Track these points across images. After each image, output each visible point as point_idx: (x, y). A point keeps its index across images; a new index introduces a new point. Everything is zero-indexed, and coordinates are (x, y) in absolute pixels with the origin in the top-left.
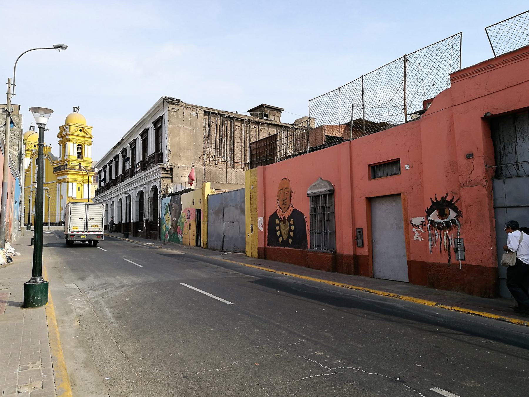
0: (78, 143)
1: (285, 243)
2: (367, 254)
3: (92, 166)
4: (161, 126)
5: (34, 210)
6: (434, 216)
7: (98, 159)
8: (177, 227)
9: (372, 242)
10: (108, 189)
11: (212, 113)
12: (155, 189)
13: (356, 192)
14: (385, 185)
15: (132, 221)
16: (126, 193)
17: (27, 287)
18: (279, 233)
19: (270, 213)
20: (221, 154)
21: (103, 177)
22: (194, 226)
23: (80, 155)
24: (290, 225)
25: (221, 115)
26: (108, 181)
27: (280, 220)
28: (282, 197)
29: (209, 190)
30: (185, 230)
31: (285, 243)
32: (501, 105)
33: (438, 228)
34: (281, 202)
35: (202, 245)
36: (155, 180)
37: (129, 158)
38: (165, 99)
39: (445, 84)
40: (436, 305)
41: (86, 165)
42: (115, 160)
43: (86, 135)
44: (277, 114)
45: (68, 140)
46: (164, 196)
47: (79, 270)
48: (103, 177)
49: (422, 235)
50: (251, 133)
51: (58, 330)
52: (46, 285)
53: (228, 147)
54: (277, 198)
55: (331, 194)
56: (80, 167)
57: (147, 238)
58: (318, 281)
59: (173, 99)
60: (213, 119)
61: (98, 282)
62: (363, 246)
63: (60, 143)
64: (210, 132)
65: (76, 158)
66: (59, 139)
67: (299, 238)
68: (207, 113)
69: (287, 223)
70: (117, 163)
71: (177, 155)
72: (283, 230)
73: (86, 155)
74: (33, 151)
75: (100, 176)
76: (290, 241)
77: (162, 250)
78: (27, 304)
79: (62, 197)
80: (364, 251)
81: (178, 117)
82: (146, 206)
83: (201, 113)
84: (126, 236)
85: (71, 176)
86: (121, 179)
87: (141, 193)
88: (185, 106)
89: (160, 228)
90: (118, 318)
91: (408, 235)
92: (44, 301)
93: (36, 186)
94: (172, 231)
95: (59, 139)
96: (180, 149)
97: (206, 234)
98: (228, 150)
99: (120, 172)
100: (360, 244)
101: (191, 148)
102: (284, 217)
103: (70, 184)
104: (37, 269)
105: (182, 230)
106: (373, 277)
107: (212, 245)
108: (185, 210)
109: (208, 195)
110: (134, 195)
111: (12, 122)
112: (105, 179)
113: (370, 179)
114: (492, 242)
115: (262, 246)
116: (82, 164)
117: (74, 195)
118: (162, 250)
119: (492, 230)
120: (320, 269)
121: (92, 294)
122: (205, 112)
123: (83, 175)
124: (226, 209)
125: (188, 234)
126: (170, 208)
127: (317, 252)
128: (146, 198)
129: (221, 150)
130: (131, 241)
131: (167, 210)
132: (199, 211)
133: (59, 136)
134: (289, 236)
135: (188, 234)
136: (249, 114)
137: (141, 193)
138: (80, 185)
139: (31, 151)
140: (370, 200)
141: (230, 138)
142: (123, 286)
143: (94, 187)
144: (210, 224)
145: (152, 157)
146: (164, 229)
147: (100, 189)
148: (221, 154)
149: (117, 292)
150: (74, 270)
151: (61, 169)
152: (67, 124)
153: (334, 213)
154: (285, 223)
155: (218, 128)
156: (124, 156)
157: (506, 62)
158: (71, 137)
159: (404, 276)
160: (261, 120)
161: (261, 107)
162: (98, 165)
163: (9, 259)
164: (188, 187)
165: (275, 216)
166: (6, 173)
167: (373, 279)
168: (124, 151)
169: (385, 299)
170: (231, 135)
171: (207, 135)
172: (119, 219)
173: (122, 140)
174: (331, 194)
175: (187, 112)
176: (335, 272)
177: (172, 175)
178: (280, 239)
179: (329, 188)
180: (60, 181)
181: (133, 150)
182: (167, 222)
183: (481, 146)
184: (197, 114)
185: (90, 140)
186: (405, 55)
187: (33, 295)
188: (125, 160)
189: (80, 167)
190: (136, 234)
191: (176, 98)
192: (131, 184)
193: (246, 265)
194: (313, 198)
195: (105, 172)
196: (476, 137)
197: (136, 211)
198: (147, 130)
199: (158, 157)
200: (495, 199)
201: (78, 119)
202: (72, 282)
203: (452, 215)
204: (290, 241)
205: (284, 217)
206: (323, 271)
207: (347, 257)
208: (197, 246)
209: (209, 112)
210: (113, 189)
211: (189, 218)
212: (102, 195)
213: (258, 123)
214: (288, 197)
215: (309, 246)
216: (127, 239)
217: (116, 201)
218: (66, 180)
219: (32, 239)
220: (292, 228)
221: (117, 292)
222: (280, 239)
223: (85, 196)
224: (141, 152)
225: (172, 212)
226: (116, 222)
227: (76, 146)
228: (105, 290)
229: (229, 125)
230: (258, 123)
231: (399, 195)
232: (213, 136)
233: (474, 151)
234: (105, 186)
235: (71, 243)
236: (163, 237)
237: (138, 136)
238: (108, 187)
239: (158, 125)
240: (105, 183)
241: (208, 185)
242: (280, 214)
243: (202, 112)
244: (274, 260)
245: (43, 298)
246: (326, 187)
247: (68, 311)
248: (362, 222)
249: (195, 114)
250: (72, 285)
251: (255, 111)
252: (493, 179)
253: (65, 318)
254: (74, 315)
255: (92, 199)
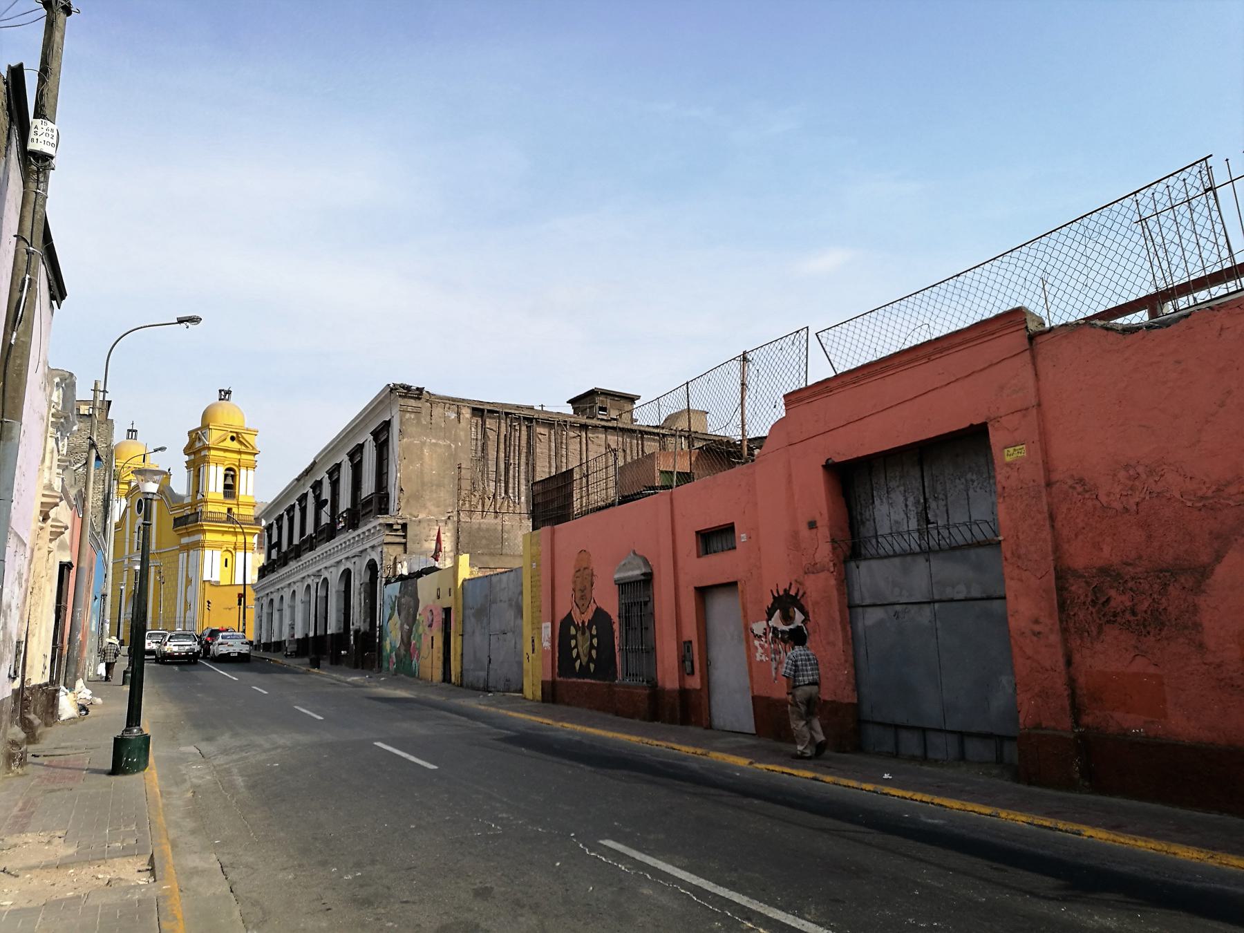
0: (228, 464)
1: (585, 671)
2: (699, 687)
3: (251, 512)
4: (387, 440)
5: (130, 610)
6: (776, 621)
7: (269, 496)
8: (409, 643)
9: (707, 664)
10: (285, 564)
11: (489, 411)
12: (372, 566)
13: (682, 577)
14: (717, 567)
15: (329, 632)
16: (318, 574)
17: (119, 743)
18: (574, 655)
19: (561, 615)
20: (506, 492)
21: (275, 540)
22: (439, 642)
23: (230, 490)
24: (592, 637)
25: (507, 414)
26: (285, 547)
27: (577, 627)
28: (579, 587)
29: (465, 572)
30: (425, 650)
31: (585, 671)
32: (848, 447)
33: (783, 640)
34: (579, 594)
35: (453, 679)
36: (373, 547)
37: (326, 501)
38: (392, 389)
39: (781, 412)
40: (751, 763)
41: (244, 511)
42: (330, 478)
43: (243, 448)
44: (627, 407)
45: (205, 460)
46: (388, 582)
47: (204, 724)
48: (275, 540)
49: (766, 652)
50: (571, 447)
51: (161, 802)
52: (147, 739)
53: (523, 476)
54: (572, 586)
55: (647, 580)
56: (230, 518)
57: (356, 667)
58: (610, 734)
59: (408, 388)
60: (490, 423)
61: (236, 742)
62: (693, 673)
63: (189, 465)
64: (484, 448)
65: (222, 497)
66: (187, 458)
67: (605, 665)
68: (480, 411)
69: (587, 634)
70: (303, 511)
71: (417, 497)
72: (582, 647)
73: (242, 491)
74: (133, 484)
75: (270, 537)
76: (592, 666)
77: (374, 690)
78: (118, 768)
79: (189, 581)
80: (694, 682)
81: (419, 422)
82: (357, 600)
83: (467, 413)
84: (315, 664)
85: (209, 537)
86: (310, 544)
87: (347, 574)
88: (434, 400)
89: (380, 647)
90: (252, 787)
91: (750, 649)
92: (142, 764)
93: (138, 567)
94: (402, 652)
95: (187, 458)
96: (423, 484)
97: (459, 658)
98: (523, 482)
99: (310, 530)
100: (689, 670)
101: (446, 481)
102: (583, 623)
103: (208, 552)
104: (134, 716)
105: (419, 649)
106: (710, 727)
107: (469, 678)
108: (425, 609)
109: (465, 580)
110: (334, 576)
111: (98, 458)
112: (279, 544)
113: (698, 556)
114: (846, 661)
115: (549, 678)
116: (235, 510)
117: (216, 578)
118: (374, 690)
119: (845, 642)
120: (632, 718)
121: (221, 760)
122: (474, 409)
123: (235, 534)
124: (494, 606)
125: (429, 661)
126: (398, 606)
127: (628, 687)
128: (356, 583)
129: (507, 483)
130: (326, 676)
131: (392, 609)
132: (447, 611)
133: (187, 451)
134: (590, 659)
135: (429, 661)
136: (569, 410)
137: (347, 574)
138: (228, 556)
139: (129, 483)
140: (703, 593)
141: (527, 460)
142: (276, 748)
143: (257, 559)
144: (466, 636)
145: (368, 502)
146: (388, 647)
147: (269, 565)
148: (506, 492)
149: (264, 757)
150: (197, 726)
151: (189, 520)
152: (205, 426)
153: (652, 614)
154: (583, 633)
155: (502, 440)
156: (317, 497)
157: (844, 385)
158: (213, 452)
159: (750, 727)
160: (589, 422)
161: (592, 393)
162: (267, 513)
163: (83, 708)
164: (432, 563)
165: (568, 620)
166: (83, 551)
167: (709, 732)
168: (317, 486)
169: (685, 759)
170: (528, 453)
171: (479, 454)
172: (304, 627)
173: (314, 464)
174: (647, 580)
175: (438, 411)
176: (652, 720)
177: (405, 537)
178: (577, 664)
179: (643, 570)
180: (187, 548)
181: (335, 484)
182: (393, 638)
183: (825, 512)
184: (459, 414)
185: (251, 457)
186: (745, 353)
187: (127, 755)
188: (320, 504)
189: (230, 518)
190: (336, 661)
191: (415, 384)
192: (328, 555)
193: (511, 713)
194: (623, 586)
195: (291, 520)
196: (816, 496)
197: (338, 611)
198: (338, 466)
199: (381, 502)
200: (850, 595)
201: (229, 417)
202: (191, 744)
203: (799, 617)
204: (592, 666)
205: (583, 623)
206: (637, 721)
207: (671, 692)
208: (444, 680)
209: (482, 410)
210: (293, 565)
211: (430, 626)
212: (273, 577)
213: (584, 427)
214: (588, 586)
215: (620, 676)
216: (316, 670)
217: (287, 594)
218: (199, 546)
219: (125, 672)
220: (595, 641)
221: (264, 757)
222: (577, 664)
223: (239, 581)
224: (347, 493)
225: (403, 615)
226: (299, 635)
227: (221, 471)
228: (244, 754)
229: (524, 433)
230: (584, 427)
231: (734, 584)
232: (490, 457)
233: (818, 518)
234: (279, 558)
235: (165, 659)
236: (385, 665)
237: (343, 458)
238: (284, 560)
239: (382, 435)
240: (279, 551)
241: (464, 559)
242: (578, 618)
243: (469, 411)
244: (568, 704)
245: (142, 760)
246: (639, 568)
247: (179, 781)
248: (690, 633)
249: (453, 416)
250: (192, 749)
251: (582, 402)
252: (845, 562)
253: (174, 789)
254: (188, 785)
255: (252, 585)
